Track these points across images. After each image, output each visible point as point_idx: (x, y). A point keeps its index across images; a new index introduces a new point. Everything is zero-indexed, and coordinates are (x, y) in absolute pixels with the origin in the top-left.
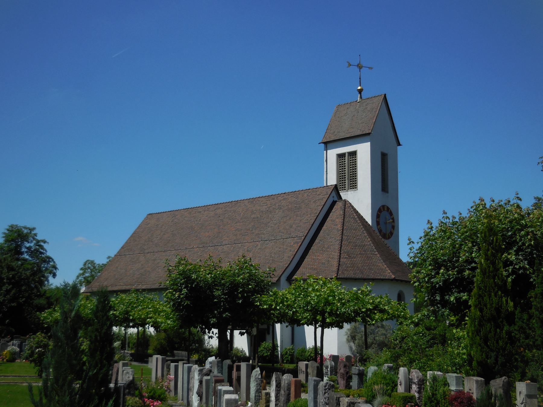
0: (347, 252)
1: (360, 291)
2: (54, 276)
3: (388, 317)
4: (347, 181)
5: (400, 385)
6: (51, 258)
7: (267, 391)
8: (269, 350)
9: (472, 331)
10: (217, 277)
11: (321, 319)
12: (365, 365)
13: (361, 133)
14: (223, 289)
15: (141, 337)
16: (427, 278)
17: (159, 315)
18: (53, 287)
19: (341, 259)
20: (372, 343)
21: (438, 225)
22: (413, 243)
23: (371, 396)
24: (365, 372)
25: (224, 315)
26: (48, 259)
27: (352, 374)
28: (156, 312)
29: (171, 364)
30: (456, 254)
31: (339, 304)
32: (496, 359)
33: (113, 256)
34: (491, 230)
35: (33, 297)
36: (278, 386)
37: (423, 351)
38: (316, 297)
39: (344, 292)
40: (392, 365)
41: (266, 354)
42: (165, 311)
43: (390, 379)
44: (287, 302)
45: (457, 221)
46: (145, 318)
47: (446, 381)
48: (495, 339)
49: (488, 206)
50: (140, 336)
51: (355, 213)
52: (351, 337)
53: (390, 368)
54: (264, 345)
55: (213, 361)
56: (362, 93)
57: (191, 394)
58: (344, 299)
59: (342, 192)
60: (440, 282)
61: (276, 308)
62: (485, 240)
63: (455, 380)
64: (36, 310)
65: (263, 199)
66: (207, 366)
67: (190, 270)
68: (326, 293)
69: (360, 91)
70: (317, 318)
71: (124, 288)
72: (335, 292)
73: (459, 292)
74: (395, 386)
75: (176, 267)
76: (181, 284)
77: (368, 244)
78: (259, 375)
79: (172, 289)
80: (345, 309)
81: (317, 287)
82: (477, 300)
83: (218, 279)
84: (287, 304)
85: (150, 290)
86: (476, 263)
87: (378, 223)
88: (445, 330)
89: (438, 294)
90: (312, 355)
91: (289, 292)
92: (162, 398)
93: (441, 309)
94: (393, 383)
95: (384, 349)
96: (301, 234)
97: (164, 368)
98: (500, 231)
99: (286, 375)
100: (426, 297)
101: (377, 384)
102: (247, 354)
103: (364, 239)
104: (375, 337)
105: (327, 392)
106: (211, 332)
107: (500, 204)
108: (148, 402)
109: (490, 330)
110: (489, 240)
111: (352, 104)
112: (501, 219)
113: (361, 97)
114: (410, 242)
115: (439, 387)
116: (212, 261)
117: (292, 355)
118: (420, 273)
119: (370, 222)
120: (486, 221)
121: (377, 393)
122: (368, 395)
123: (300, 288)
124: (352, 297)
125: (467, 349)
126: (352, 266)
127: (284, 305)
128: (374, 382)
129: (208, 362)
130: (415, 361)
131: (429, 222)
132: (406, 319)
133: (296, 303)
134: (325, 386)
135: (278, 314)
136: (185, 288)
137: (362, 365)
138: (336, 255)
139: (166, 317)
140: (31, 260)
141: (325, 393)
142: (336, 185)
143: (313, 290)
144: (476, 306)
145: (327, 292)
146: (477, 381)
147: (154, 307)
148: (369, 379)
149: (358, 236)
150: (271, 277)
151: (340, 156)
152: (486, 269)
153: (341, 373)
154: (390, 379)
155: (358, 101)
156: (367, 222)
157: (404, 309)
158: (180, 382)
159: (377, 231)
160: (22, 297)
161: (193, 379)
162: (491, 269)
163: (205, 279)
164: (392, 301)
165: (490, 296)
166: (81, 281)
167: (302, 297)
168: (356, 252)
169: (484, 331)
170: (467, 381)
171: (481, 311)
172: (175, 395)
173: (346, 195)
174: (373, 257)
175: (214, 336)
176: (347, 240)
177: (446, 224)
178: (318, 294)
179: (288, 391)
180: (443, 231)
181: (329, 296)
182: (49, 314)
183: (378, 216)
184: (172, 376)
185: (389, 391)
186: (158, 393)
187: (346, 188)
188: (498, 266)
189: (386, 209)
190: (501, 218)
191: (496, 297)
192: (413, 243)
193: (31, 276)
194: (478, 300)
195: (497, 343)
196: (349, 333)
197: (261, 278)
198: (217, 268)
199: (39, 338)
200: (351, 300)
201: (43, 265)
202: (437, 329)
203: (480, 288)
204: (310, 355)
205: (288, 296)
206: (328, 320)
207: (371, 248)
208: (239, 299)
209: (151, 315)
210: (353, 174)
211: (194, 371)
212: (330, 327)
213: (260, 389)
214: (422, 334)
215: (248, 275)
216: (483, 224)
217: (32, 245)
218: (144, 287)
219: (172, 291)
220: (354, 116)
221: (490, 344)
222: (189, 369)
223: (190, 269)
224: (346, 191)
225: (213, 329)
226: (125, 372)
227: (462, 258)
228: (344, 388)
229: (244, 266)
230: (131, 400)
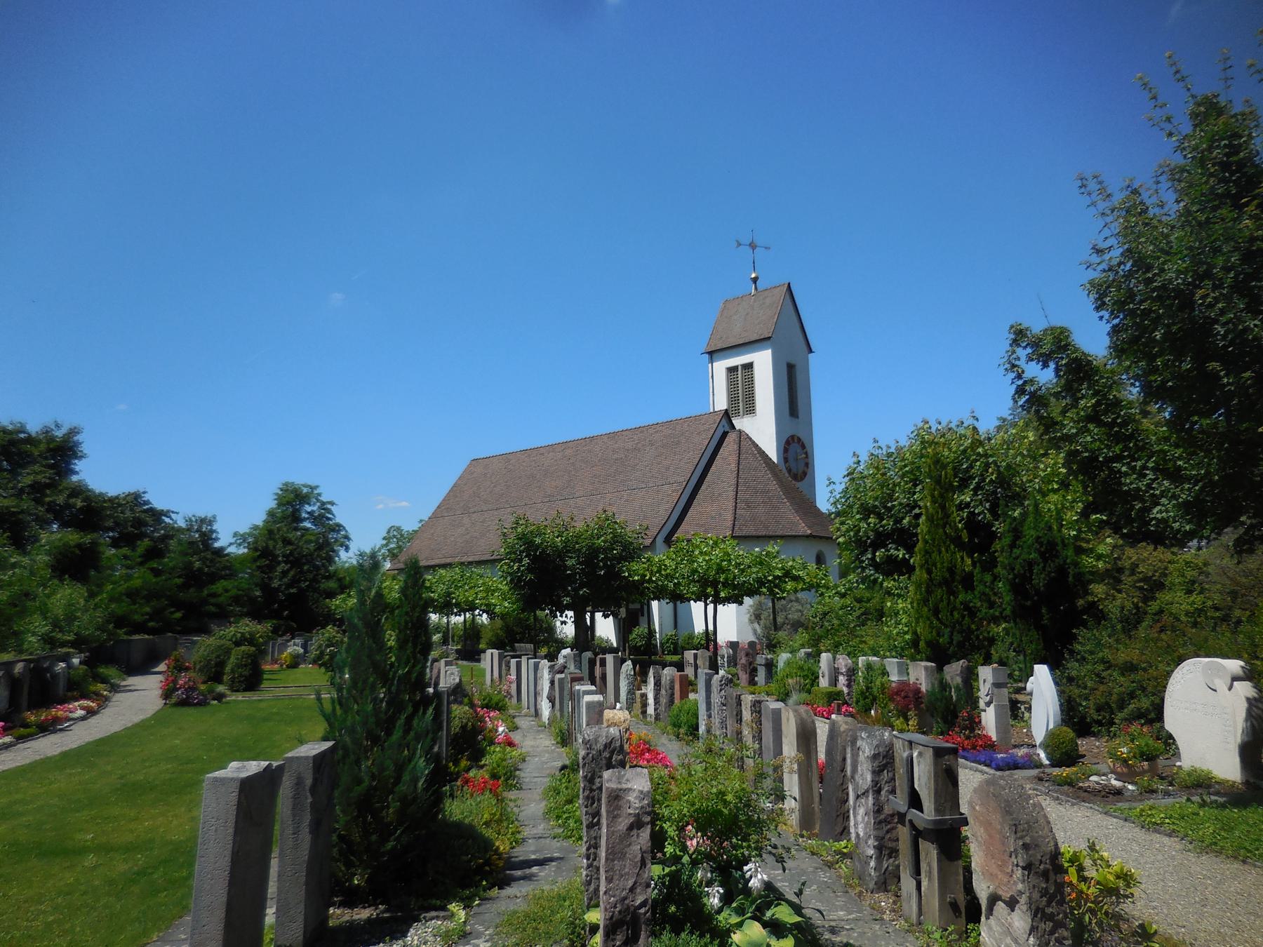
4: (741, 404)
13: (755, 337)
14: (578, 557)
26: (338, 528)
36: (658, 684)
37: (852, 632)
44: (665, 570)
53: (808, 655)
57: (539, 699)
61: (650, 578)
66: (561, 660)
69: (755, 280)
71: (443, 561)
76: (520, 552)
87: (786, 460)
94: (812, 675)
95: (800, 630)
96: (682, 479)
102: (615, 645)
106: (564, 615)
111: (744, 299)
113: (756, 288)
117: (675, 644)
119: (775, 459)
131: (854, 454)
134: (721, 681)
136: (526, 557)
138: (731, 504)
141: (721, 690)
143: (701, 553)
144: (922, 567)
146: (926, 668)
154: (809, 669)
159: (784, 470)
160: (305, 581)
165: (940, 552)
171: (929, 572)
175: (568, 620)
181: (722, 561)
183: (786, 450)
184: (513, 677)
186: (495, 699)
187: (741, 413)
189: (796, 441)
192: (834, 483)
193: (315, 550)
195: (952, 615)
203: (926, 542)
205: (667, 562)
206: (722, 595)
220: (747, 314)
228: (747, 685)
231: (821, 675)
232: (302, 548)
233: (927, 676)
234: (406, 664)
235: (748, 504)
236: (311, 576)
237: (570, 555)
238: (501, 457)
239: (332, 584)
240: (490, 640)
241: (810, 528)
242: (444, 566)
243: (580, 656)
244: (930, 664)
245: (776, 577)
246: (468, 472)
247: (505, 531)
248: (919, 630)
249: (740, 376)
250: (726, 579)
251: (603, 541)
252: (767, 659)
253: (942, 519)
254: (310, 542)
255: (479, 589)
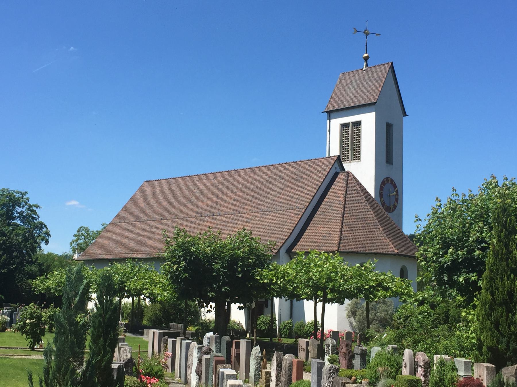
0: (349, 225)
1: (364, 268)
2: (47, 242)
3: (392, 294)
4: (350, 152)
5: (405, 367)
6: (44, 225)
7: (267, 370)
8: (267, 324)
9: (483, 315)
10: (216, 250)
11: (322, 295)
12: (368, 344)
13: (364, 102)
14: (223, 263)
15: (135, 307)
16: (436, 257)
17: (155, 286)
18: (45, 253)
19: (343, 232)
20: (373, 319)
21: (447, 203)
22: (420, 221)
23: (375, 378)
24: (368, 352)
25: (223, 290)
26: (41, 225)
27: (355, 354)
28: (153, 283)
29: (169, 339)
30: (465, 233)
31: (342, 281)
32: (508, 345)
33: (108, 223)
34: (504, 209)
35: (24, 264)
36: (279, 366)
37: (428, 332)
38: (318, 273)
39: (347, 268)
40: (396, 346)
41: (264, 328)
42: (162, 282)
43: (395, 360)
44: (288, 277)
45: (467, 199)
46: (140, 289)
47: (455, 366)
48: (507, 324)
49: (500, 184)
50: (134, 305)
51: (358, 185)
52: (352, 312)
53: (395, 349)
54: (262, 318)
55: (211, 337)
56: (368, 60)
57: (189, 371)
58: (346, 276)
59: (344, 163)
60: (449, 262)
61: (276, 282)
62: (497, 220)
63: (464, 366)
64: (27, 277)
65: (263, 169)
66: (205, 342)
67: (189, 242)
68: (329, 270)
69: (366, 59)
70: (318, 293)
71: (118, 256)
72: (338, 268)
73: (468, 273)
74: (399, 367)
75: (174, 239)
76: (179, 256)
77: (371, 217)
78: (259, 354)
79: (170, 261)
80: (348, 285)
81: (319, 262)
82: (488, 283)
83: (218, 252)
84: (288, 279)
85: (146, 260)
86: (486, 243)
87: (381, 196)
88: (449, 307)
89: (445, 274)
90: (311, 330)
91: (290, 267)
92: (159, 376)
93: (449, 289)
94: (397, 365)
95: (388, 328)
96: (302, 206)
97: (161, 343)
98: (513, 210)
99: (287, 355)
100: (433, 277)
101: (381, 366)
102: (245, 328)
103: (367, 212)
104: (376, 313)
105: (332, 376)
106: (209, 306)
107: (513, 182)
108: (145, 379)
109: (502, 314)
110: (503, 221)
111: (357, 72)
112: (514, 198)
113: (367, 65)
114: (417, 220)
115: (447, 372)
116: (211, 233)
117: (290, 330)
118: (428, 252)
119: (373, 195)
120: (499, 200)
121: (381, 375)
122: (371, 377)
123: (302, 263)
124: (355, 273)
125: (477, 333)
126: (354, 239)
127: (284, 280)
128: (378, 363)
129: (206, 337)
130: (420, 342)
131: (437, 199)
132: (410, 296)
133: (297, 279)
134: (330, 370)
135: (278, 288)
136: (183, 260)
137: (364, 345)
138: (338, 227)
139: (162, 288)
140: (22, 226)
141: (329, 377)
142: (339, 156)
143: (315, 265)
144: (487, 290)
145: (330, 268)
146: (487, 368)
147: (150, 279)
148: (372, 360)
149: (361, 209)
150: (271, 251)
151: (344, 126)
152: (498, 251)
153: (343, 352)
154: (395, 360)
155: (364, 69)
156: (370, 195)
157: (408, 287)
158: (178, 358)
159: (380, 204)
160: (13, 264)
161: (191, 356)
162: (504, 252)
163: (204, 251)
164: (396, 278)
165: (502, 279)
166: (74, 248)
167: (303, 273)
168: (358, 225)
169: (495, 315)
170: (477, 367)
171: (493, 294)
172: (172, 372)
173: (349, 166)
174: (376, 231)
175: (212, 310)
176: (349, 213)
177: (455, 202)
178: (320, 270)
179: (290, 372)
180: (452, 209)
181: (331, 272)
182: (40, 282)
183: (381, 189)
184: (170, 353)
185: (394, 374)
186: (156, 369)
187: (350, 159)
188: (511, 249)
189: (390, 181)
190: (514, 197)
191: (509, 280)
192: (420, 220)
193: (22, 242)
194: (489, 283)
195: (509, 328)
196: (349, 308)
197: (261, 252)
198: (216, 241)
199: (32, 309)
200: (354, 276)
201: (35, 231)
202: (440, 305)
203: (491, 271)
204: (308, 330)
205: (290, 271)
206: (329, 296)
207: (373, 222)
208: (239, 273)
209: (147, 286)
210: (357, 145)
211: (193, 348)
212: (331, 302)
213: (260, 367)
214: (427, 313)
215: (248, 248)
216: (495, 203)
217: (24, 210)
218: (139, 256)
219: (171, 263)
220: (359, 84)
221: (501, 329)
222: (188, 346)
223: (189, 242)
224: (349, 162)
225: (211, 303)
226: (122, 349)
227: (472, 238)
228: (346, 368)
229: (244, 239)
230: (129, 380)
231: (404, 366)
232: (12, 239)
233: (488, 375)
234: (98, 355)
235: (350, 226)
236: (18, 261)
237: (216, 261)
238: (167, 181)
239: (34, 268)
240: (150, 318)
241: (397, 248)
242: (119, 260)
243: (220, 338)
244: (490, 365)
245: (371, 287)
246: (141, 192)
247: (169, 240)
248: (482, 337)
249: (350, 130)
250: (334, 286)
251: (241, 252)
252: (362, 350)
253: (505, 254)
254: (18, 235)
255: (145, 281)
